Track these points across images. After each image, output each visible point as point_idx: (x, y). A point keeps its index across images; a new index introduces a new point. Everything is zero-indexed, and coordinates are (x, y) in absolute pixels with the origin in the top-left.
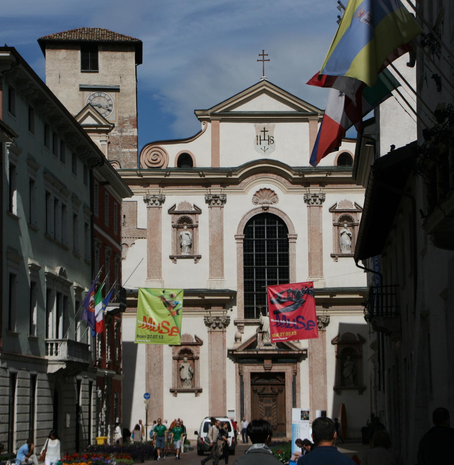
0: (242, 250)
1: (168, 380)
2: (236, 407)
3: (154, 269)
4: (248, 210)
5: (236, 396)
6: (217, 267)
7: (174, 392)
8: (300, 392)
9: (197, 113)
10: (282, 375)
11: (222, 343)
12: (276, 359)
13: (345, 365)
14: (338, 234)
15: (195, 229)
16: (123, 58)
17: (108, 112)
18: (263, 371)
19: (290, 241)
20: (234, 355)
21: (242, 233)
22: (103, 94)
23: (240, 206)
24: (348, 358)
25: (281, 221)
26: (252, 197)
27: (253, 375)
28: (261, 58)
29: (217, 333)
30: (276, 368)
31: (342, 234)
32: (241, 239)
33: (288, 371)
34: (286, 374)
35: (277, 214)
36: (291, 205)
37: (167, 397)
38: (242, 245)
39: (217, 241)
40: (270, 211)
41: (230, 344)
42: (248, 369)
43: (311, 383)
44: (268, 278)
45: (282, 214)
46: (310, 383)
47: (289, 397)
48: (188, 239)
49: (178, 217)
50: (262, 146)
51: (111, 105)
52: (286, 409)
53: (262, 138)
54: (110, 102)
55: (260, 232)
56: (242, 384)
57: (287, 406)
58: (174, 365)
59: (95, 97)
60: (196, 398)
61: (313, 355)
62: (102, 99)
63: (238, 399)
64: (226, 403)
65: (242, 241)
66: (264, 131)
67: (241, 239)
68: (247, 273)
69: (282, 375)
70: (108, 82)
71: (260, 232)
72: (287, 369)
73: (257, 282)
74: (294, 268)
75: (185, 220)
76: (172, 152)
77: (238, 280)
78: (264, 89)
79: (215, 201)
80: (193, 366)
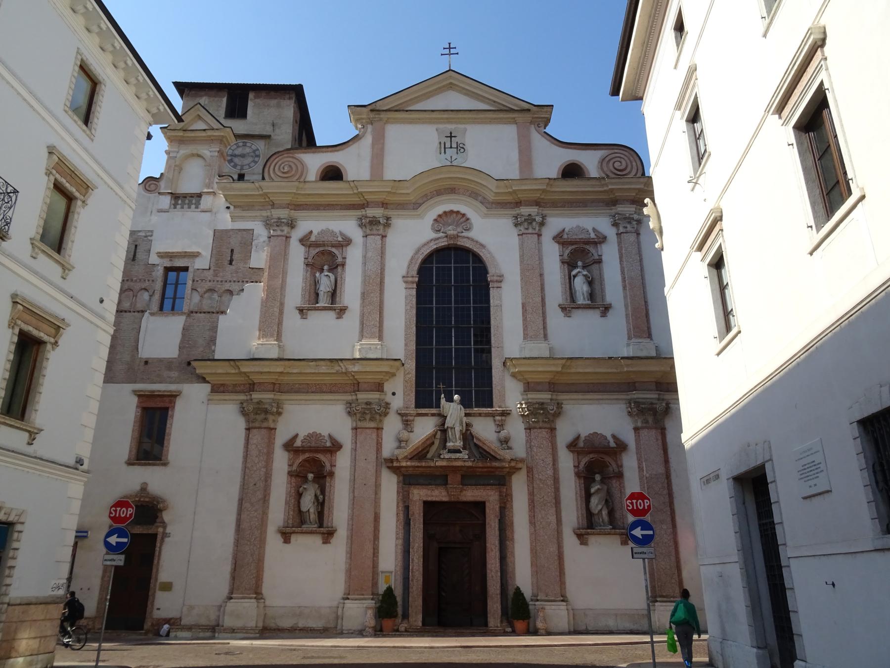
0: (414, 300)
1: (278, 511)
3: (271, 322)
5: (396, 545)
6: (373, 323)
7: (286, 536)
8: (512, 540)
10: (480, 506)
11: (375, 449)
12: (469, 477)
13: (593, 490)
14: (570, 278)
15: (339, 269)
16: (278, 106)
18: (445, 499)
20: (391, 464)
21: (415, 273)
22: (249, 142)
23: (412, 237)
25: (477, 258)
26: (431, 222)
27: (428, 505)
28: (447, 51)
29: (368, 431)
30: (471, 494)
31: (575, 276)
32: (413, 282)
33: (491, 499)
34: (487, 504)
35: (471, 247)
36: (495, 239)
37: (273, 541)
38: (414, 292)
39: (375, 286)
41: (389, 448)
42: (420, 494)
43: (532, 522)
46: (531, 522)
47: (493, 547)
48: (328, 283)
49: (314, 251)
50: (448, 156)
52: (488, 571)
53: (448, 145)
56: (407, 523)
57: (489, 566)
58: (289, 486)
59: (238, 147)
60: (325, 545)
61: (535, 472)
63: (399, 551)
64: (377, 557)
65: (415, 286)
66: (451, 137)
67: (413, 282)
69: (480, 506)
72: (490, 496)
75: (326, 257)
77: (406, 345)
78: (451, 83)
79: (375, 226)
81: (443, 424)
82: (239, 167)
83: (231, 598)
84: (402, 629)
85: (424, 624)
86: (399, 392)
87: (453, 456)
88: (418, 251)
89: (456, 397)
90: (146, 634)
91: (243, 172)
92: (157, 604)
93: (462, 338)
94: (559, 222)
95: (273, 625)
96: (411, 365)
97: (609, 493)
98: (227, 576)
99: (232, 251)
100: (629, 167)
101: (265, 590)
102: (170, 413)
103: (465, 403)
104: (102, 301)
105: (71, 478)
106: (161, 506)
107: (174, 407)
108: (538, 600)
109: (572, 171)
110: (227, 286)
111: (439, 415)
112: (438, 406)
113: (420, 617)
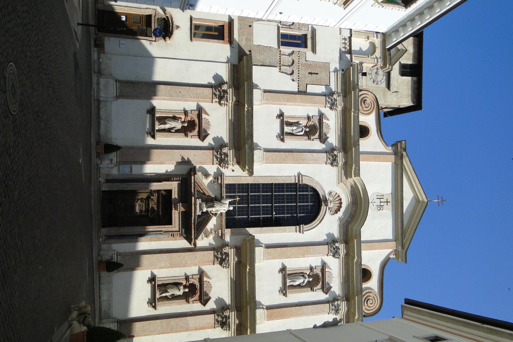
2: (135, 175)
4: (324, 187)
9: (403, 142)
12: (186, 217)
17: (372, 80)
19: (298, 227)
24: (187, 290)
27: (169, 192)
30: (176, 215)
32: (299, 181)
38: (293, 181)
40: (323, 208)
44: (263, 206)
45: (321, 219)
51: (377, 84)
52: (133, 227)
53: (382, 200)
54: (379, 83)
55: (304, 199)
57: (136, 228)
62: (382, 77)
66: (387, 202)
67: (299, 181)
68: (268, 187)
70: (393, 82)
71: (304, 199)
73: (259, 196)
74: (273, 232)
75: (314, 129)
76: (369, 120)
80: (178, 131)
81: (216, 200)
82: (370, 72)
83: (116, 82)
84: (191, 326)
85: (104, 192)
86: (234, 173)
87: (198, 206)
88: (317, 183)
89: (231, 208)
90: (95, 34)
91: (367, 75)
92: (112, 39)
93: (266, 210)
94: (335, 267)
95: (101, 106)
96: (250, 180)
97: (165, 14)
98: (129, 79)
99: (317, 74)
100: (370, 309)
101: (121, 101)
102: (221, 41)
103: (228, 213)
104: (281, 13)
105: (181, 3)
106: (167, 38)
107: (224, 43)
108: (117, 256)
109: (366, 274)
110: (296, 72)
111: (222, 198)
112: (228, 197)
113: (107, 189)
